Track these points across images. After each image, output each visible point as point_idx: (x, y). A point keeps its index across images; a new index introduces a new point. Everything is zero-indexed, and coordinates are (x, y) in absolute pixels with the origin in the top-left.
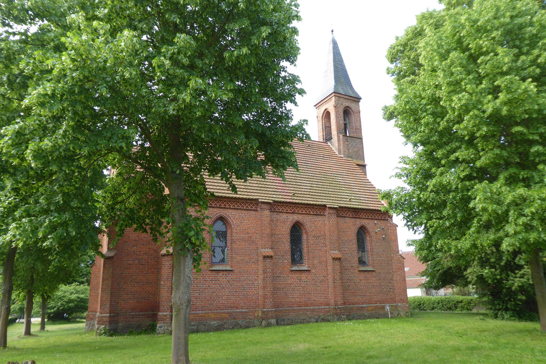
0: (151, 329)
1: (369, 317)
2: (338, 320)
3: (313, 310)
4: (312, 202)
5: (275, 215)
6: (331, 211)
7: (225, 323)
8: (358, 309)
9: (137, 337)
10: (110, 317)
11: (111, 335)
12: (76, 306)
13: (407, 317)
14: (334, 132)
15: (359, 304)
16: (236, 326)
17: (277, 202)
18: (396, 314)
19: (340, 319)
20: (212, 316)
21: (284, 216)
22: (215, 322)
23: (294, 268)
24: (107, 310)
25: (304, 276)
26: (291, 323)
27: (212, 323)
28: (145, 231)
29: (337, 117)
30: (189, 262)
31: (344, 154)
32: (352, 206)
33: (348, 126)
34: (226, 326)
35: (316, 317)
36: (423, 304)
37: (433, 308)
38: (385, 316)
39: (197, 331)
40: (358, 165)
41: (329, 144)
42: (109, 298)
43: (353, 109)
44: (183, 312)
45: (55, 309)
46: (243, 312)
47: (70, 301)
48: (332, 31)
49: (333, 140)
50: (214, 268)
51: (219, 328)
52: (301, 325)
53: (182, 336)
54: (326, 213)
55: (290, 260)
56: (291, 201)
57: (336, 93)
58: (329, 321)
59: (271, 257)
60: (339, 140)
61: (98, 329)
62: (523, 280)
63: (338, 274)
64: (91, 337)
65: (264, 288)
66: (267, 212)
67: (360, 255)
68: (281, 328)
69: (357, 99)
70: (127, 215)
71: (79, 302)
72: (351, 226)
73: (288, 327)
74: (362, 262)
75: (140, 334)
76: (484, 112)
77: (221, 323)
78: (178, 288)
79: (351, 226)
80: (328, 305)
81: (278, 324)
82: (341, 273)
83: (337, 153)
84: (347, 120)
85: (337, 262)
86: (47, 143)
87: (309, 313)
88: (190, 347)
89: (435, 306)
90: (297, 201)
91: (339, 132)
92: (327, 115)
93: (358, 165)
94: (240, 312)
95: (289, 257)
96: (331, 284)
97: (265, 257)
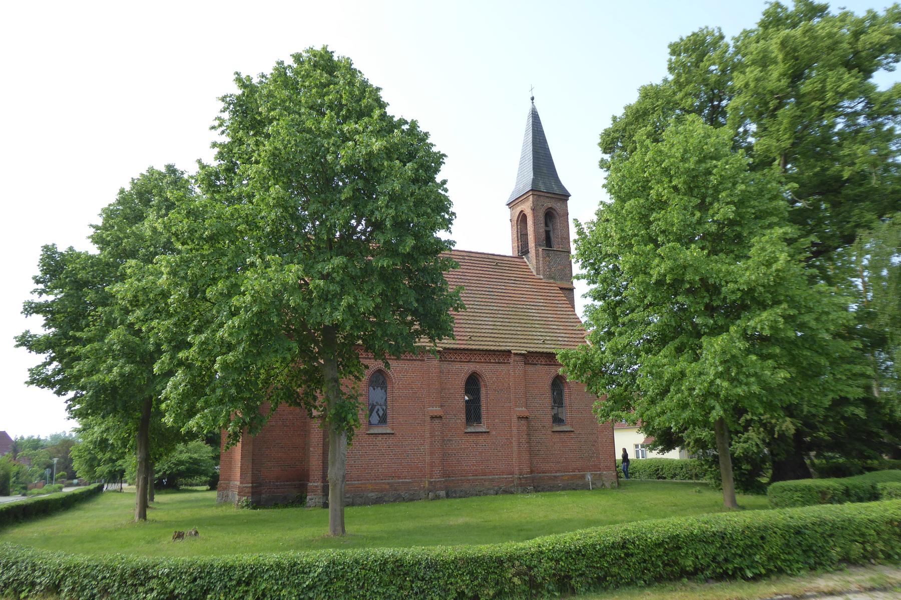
0: (299, 501)
1: (564, 489)
2: (522, 492)
3: (492, 480)
4: (493, 348)
5: (445, 366)
6: (517, 358)
7: (385, 495)
8: (550, 478)
9: (286, 510)
10: (252, 487)
11: (254, 508)
12: (188, 469)
13: (613, 488)
14: (532, 245)
15: (551, 472)
16: (398, 499)
17: (448, 349)
18: (599, 485)
19: (525, 491)
20: (370, 487)
21: (457, 366)
22: (373, 494)
23: (469, 430)
24: (249, 479)
25: (481, 438)
26: (466, 495)
27: (370, 495)
28: (299, 404)
29: (535, 224)
30: (344, 440)
31: (544, 275)
32: (545, 350)
33: (551, 234)
34: (386, 499)
35: (496, 488)
36: (662, 469)
37: (674, 476)
38: (585, 487)
39: (352, 504)
40: (561, 289)
41: (525, 260)
42: (250, 466)
43: (559, 210)
44: (339, 487)
45: (161, 473)
46: (407, 483)
47: (181, 463)
48: (533, 99)
49: (530, 255)
50: (372, 431)
51: (378, 501)
52: (474, 498)
53: (338, 508)
54: (511, 361)
55: (464, 420)
56: (466, 347)
57: (534, 190)
58: (512, 493)
59: (440, 417)
60: (537, 255)
61: (239, 501)
62: (746, 445)
63: (525, 436)
64: (232, 510)
65: (432, 453)
66: (436, 362)
67: (555, 411)
68: (452, 501)
69: (564, 196)
70: (284, 394)
71: (191, 463)
72: (543, 375)
73: (458, 500)
74: (557, 420)
75: (286, 506)
76: (651, 276)
77: (380, 495)
78: (333, 464)
79: (543, 375)
80: (512, 474)
81: (448, 496)
82: (528, 435)
83: (535, 273)
84: (550, 225)
85: (523, 422)
86: (230, 357)
87: (487, 483)
88: (346, 520)
89: (677, 472)
90: (474, 347)
91: (537, 245)
92: (522, 218)
93: (561, 289)
94: (402, 482)
95: (464, 416)
96: (515, 448)
97: (432, 417)
